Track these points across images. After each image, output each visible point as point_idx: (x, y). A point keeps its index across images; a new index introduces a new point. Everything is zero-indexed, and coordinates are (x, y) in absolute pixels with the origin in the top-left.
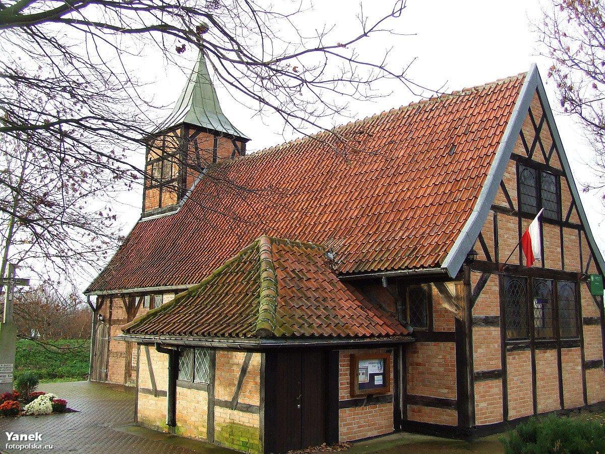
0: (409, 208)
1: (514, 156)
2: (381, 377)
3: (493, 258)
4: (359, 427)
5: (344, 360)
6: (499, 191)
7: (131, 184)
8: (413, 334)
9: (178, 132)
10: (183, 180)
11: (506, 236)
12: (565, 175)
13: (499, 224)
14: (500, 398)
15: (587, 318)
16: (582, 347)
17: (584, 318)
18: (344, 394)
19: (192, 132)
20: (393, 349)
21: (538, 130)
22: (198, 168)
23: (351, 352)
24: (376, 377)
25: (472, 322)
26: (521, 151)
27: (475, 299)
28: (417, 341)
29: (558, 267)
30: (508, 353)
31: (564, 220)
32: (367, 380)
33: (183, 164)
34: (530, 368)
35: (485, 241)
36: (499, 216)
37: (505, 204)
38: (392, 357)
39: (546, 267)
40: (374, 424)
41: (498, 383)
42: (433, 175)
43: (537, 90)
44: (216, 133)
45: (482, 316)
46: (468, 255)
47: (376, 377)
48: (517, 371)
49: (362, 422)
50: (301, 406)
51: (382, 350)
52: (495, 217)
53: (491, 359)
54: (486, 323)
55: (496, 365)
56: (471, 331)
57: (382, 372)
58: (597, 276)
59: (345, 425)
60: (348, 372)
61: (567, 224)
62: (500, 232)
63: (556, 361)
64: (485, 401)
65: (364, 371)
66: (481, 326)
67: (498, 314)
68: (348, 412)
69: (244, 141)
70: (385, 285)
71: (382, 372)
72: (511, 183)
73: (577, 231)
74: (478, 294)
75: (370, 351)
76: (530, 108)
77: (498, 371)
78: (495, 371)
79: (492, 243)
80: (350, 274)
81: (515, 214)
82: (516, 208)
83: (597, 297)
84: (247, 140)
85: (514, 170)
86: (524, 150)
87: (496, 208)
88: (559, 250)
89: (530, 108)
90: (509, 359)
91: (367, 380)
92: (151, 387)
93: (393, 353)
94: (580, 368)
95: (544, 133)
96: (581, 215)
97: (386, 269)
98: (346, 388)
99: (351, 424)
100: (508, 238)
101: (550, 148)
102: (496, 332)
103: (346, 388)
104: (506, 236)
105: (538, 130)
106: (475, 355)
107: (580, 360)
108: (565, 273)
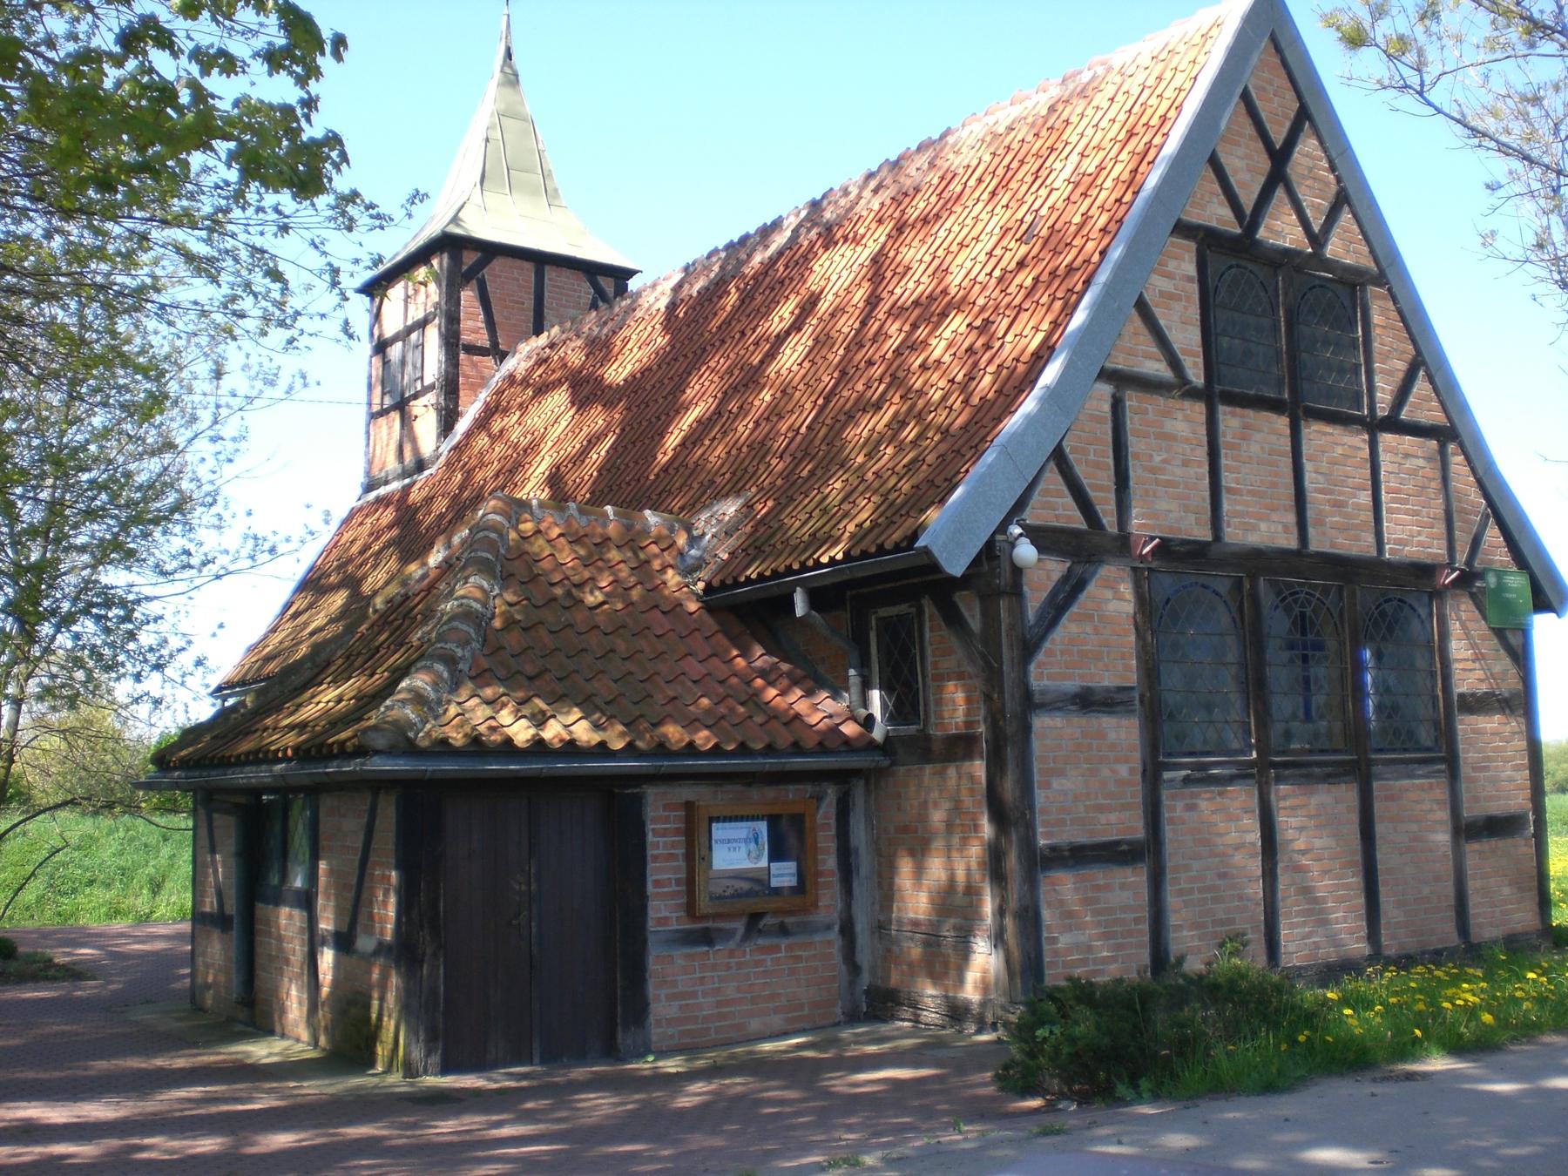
1: (1183, 229)
3: (1109, 521)
4: (719, 1004)
5: (667, 820)
6: (1128, 330)
7: (245, 361)
11: (1157, 459)
12: (1380, 279)
13: (1132, 422)
15: (1473, 695)
16: (1453, 774)
17: (1461, 696)
18: (663, 911)
21: (1280, 157)
23: (686, 792)
25: (1030, 702)
26: (1218, 215)
27: (1042, 638)
29: (1360, 545)
31: (1383, 410)
36: (1132, 400)
37: (1157, 368)
39: (1315, 545)
40: (773, 997)
41: (1135, 878)
43: (1274, 40)
45: (1071, 685)
49: (730, 990)
52: (1117, 405)
53: (1100, 809)
55: (1126, 824)
56: (1026, 729)
59: (670, 998)
60: (681, 851)
61: (1393, 424)
62: (1135, 445)
63: (1355, 817)
67: (1132, 678)
68: (680, 962)
69: (621, 275)
70: (800, 608)
72: (1178, 306)
74: (1054, 622)
77: (1129, 843)
78: (1117, 843)
79: (1107, 478)
81: (1192, 394)
83: (1509, 635)
84: (631, 273)
85: (1190, 269)
86: (1226, 213)
87: (1121, 380)
88: (1365, 498)
90: (1174, 807)
92: (1454, 939)
94: (1443, 837)
96: (1446, 391)
98: (673, 895)
99: (694, 995)
100: (1164, 461)
103: (673, 895)
104: (1157, 459)
106: (1040, 797)
107: (1444, 815)
108: (1390, 565)
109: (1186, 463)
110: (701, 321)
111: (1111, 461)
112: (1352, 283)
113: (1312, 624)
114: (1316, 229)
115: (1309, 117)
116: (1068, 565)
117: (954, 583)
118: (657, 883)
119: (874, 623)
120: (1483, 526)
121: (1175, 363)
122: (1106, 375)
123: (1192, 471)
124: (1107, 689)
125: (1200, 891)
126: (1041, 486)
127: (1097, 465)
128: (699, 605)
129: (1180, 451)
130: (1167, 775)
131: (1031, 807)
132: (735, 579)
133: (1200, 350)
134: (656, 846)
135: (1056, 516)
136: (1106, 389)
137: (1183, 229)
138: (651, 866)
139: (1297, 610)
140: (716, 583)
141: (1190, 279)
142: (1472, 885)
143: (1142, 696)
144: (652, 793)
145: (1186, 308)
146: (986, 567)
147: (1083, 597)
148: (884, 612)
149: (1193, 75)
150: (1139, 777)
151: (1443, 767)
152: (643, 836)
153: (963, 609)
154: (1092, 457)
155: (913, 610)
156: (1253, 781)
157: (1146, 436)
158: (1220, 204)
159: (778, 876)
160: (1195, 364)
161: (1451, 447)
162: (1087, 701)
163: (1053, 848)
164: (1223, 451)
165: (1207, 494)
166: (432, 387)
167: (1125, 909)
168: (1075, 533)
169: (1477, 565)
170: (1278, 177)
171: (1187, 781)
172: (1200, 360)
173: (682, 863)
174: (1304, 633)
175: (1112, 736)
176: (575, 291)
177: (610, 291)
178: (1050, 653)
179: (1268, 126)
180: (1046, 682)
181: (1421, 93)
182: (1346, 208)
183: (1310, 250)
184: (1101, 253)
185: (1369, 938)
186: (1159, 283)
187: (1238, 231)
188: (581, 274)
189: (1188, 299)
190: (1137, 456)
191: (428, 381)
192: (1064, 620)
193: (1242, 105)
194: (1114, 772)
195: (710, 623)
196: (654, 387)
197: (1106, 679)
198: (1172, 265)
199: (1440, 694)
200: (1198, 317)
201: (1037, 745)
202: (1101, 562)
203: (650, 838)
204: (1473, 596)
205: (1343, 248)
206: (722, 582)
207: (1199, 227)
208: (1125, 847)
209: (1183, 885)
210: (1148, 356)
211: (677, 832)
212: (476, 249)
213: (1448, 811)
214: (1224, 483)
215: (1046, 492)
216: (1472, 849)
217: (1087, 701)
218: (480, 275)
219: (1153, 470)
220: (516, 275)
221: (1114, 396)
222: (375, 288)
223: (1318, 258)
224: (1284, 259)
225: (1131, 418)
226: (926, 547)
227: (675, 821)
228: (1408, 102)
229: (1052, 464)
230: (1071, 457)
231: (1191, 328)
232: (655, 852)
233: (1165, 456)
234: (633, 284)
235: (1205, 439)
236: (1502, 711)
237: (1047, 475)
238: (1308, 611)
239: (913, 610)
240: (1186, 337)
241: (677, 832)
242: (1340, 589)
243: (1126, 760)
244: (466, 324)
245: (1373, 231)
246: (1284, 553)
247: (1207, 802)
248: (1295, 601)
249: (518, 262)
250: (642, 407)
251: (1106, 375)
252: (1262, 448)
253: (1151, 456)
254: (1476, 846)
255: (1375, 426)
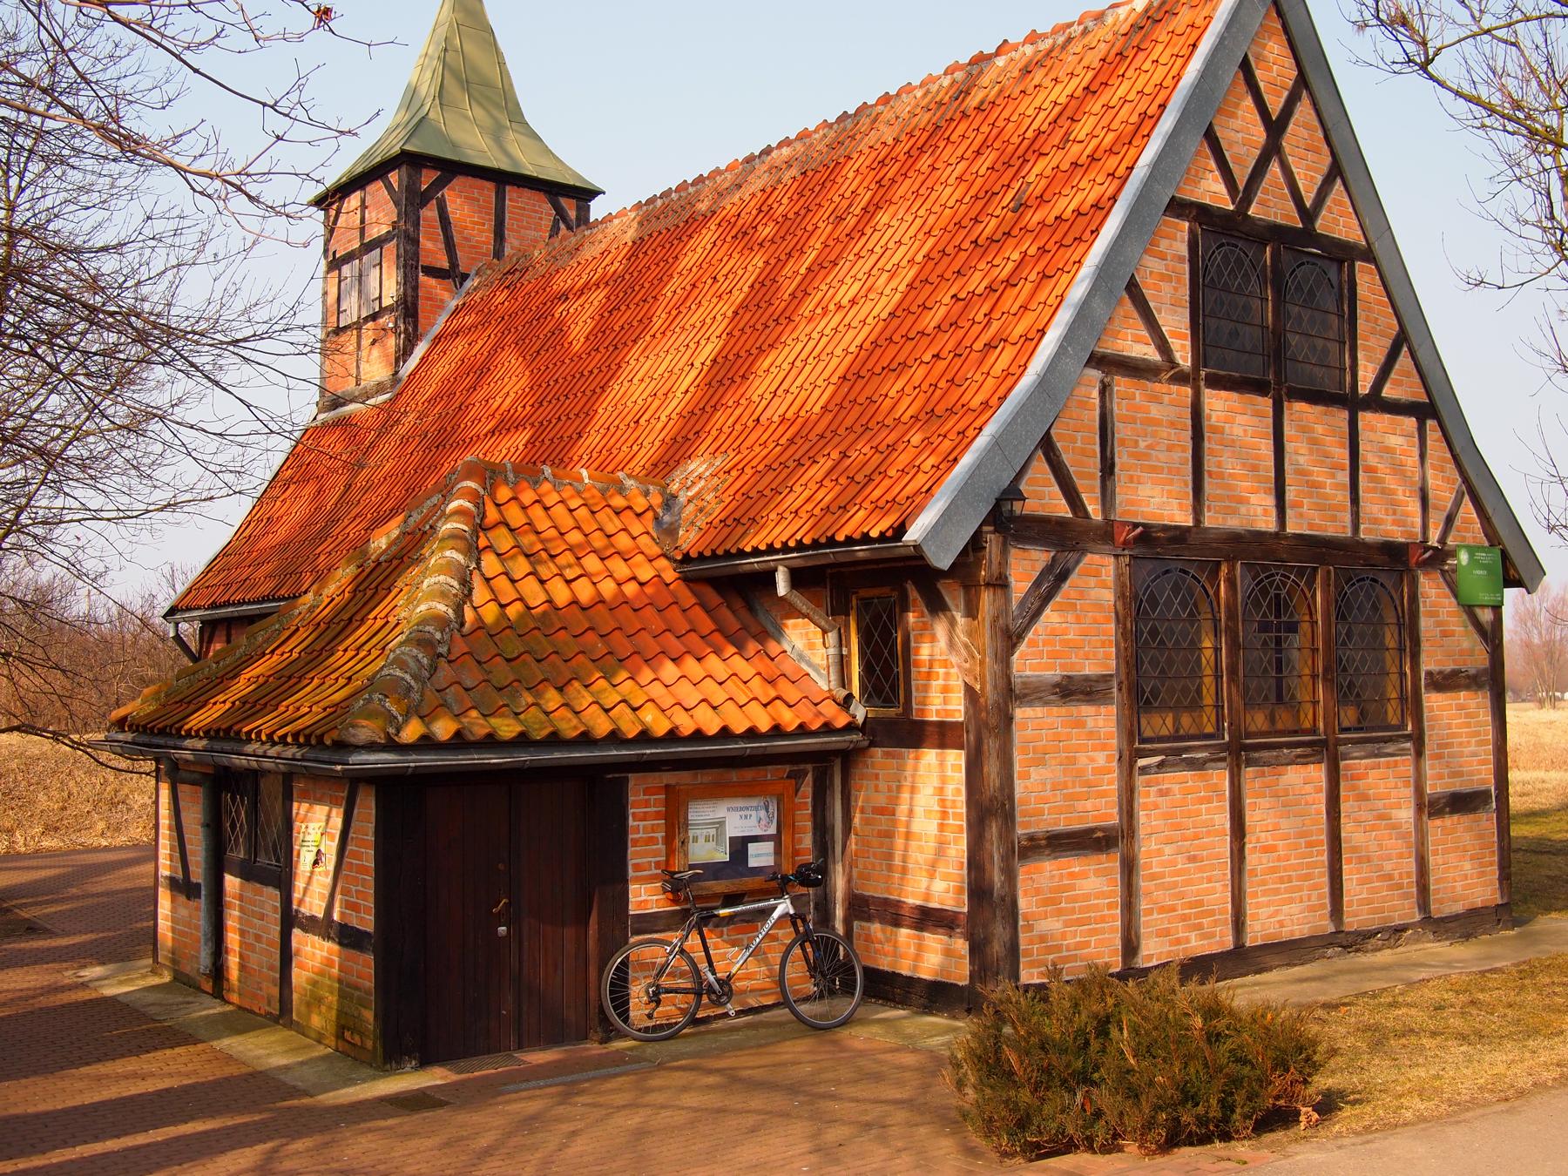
0: (883, 369)
1: (1178, 207)
2: (769, 847)
3: (1094, 510)
8: (866, 727)
9: (393, 177)
10: (409, 308)
13: (1118, 408)
14: (1110, 906)
19: (427, 178)
20: (809, 767)
21: (1276, 127)
22: (453, 275)
23: (668, 778)
24: (752, 847)
25: (1012, 694)
26: (1212, 190)
28: (873, 744)
29: (1337, 527)
30: (1140, 780)
31: (1364, 388)
32: (723, 856)
33: (411, 266)
34: (1224, 820)
35: (1067, 458)
36: (1121, 384)
38: (807, 788)
41: (1111, 863)
42: (959, 272)
44: (503, 179)
45: (1053, 674)
46: (999, 503)
47: (752, 847)
48: (1177, 827)
50: (509, 930)
51: (770, 773)
52: (1105, 389)
54: (1064, 696)
55: (1101, 810)
57: (772, 830)
58: (1481, 548)
60: (660, 835)
61: (1376, 402)
64: (1060, 913)
65: (713, 832)
66: (1047, 703)
69: (586, 194)
70: (782, 588)
71: (772, 830)
73: (1410, 423)
75: (734, 776)
76: (1246, 55)
78: (1092, 830)
80: (873, 541)
81: (1180, 378)
82: (1183, 356)
83: (1478, 611)
84: (593, 193)
86: (1221, 188)
89: (1246, 55)
90: (1147, 793)
91: (723, 856)
93: (809, 778)
95: (1301, 130)
96: (1431, 373)
97: (882, 534)
100: (1150, 447)
101: (1319, 179)
102: (1103, 720)
104: (1142, 444)
105: (1276, 127)
107: (1409, 792)
108: (1364, 544)
109: (1170, 449)
110: (671, 260)
111: (1097, 448)
112: (1343, 255)
113: (1287, 606)
114: (1308, 204)
115: (1307, 87)
116: (1052, 554)
117: (940, 574)
118: (637, 867)
119: (854, 602)
120: (1457, 504)
121: (1163, 347)
122: (1098, 361)
123: (1176, 455)
124: (1087, 678)
125: (1183, 907)
126: (1029, 475)
127: (1083, 452)
128: (677, 575)
129: (1165, 435)
130: (1142, 762)
131: (1011, 797)
132: (713, 551)
133: (1189, 332)
134: (637, 830)
135: (1042, 505)
136: (1095, 375)
137: (1178, 207)
138: (631, 850)
139: (1272, 592)
140: (693, 554)
141: (1180, 259)
142: (1432, 860)
143: (1120, 684)
144: (633, 778)
145: (1176, 289)
146: (971, 559)
147: (1066, 586)
148: (863, 593)
149: (1191, 41)
150: (1115, 764)
151: (1408, 745)
152: (626, 819)
153: (947, 599)
154: (1079, 444)
155: (895, 594)
156: (1223, 764)
157: (1133, 420)
158: (1215, 180)
159: (758, 855)
160: (1183, 346)
161: (1430, 423)
162: (1071, 690)
163: (1031, 838)
164: (1206, 435)
165: (1189, 479)
166: (390, 309)
167: (1100, 895)
168: (1061, 523)
169: (1450, 542)
170: (1272, 149)
171: (1161, 765)
172: (1188, 343)
173: (661, 846)
174: (1278, 616)
175: (1090, 723)
176: (536, 212)
177: (572, 214)
178: (1033, 644)
179: (1266, 97)
180: (1028, 673)
181: (1424, 67)
182: (1339, 181)
183: (1301, 226)
184: (1092, 232)
185: (1331, 916)
186: (1153, 264)
187: (1231, 207)
188: (542, 196)
189: (1179, 281)
190: (1123, 442)
191: (387, 302)
192: (1048, 611)
193: (1241, 75)
194: (1092, 760)
195: (688, 598)
196: (623, 328)
197: (1089, 669)
198: (1164, 245)
199: (1408, 671)
200: (1188, 298)
201: (1018, 735)
202: (1084, 552)
203: (631, 822)
204: (1443, 572)
205: (1337, 222)
206: (700, 554)
207: (1192, 204)
208: (1100, 834)
209: (1155, 870)
210: (1137, 340)
211: (657, 816)
212: (435, 168)
213: (1412, 789)
214: (1206, 468)
215: (1033, 482)
216: (1436, 827)
217: (1071, 690)
218: (439, 195)
219: (1138, 456)
220: (476, 195)
221: (1102, 382)
222: (330, 200)
223: (1307, 234)
224: (1276, 233)
225: (1118, 404)
226: (917, 547)
227: (656, 803)
228: (1416, 80)
229: (1040, 453)
230: (1059, 445)
231: (1180, 309)
232: (635, 836)
233: (1150, 441)
234: (597, 209)
235: (1189, 422)
236: (1467, 687)
237: (1035, 463)
238: (1283, 593)
239: (895, 594)
240: (1175, 323)
241: (657, 816)
242: (1315, 569)
243: (1104, 747)
244: (426, 243)
245: (1367, 203)
246: (1259, 536)
247: (1178, 781)
248: (1271, 584)
249: (479, 182)
250: (611, 349)
251: (1098, 361)
252: (1245, 431)
253: (1137, 442)
254: (1438, 822)
255: (1353, 403)
